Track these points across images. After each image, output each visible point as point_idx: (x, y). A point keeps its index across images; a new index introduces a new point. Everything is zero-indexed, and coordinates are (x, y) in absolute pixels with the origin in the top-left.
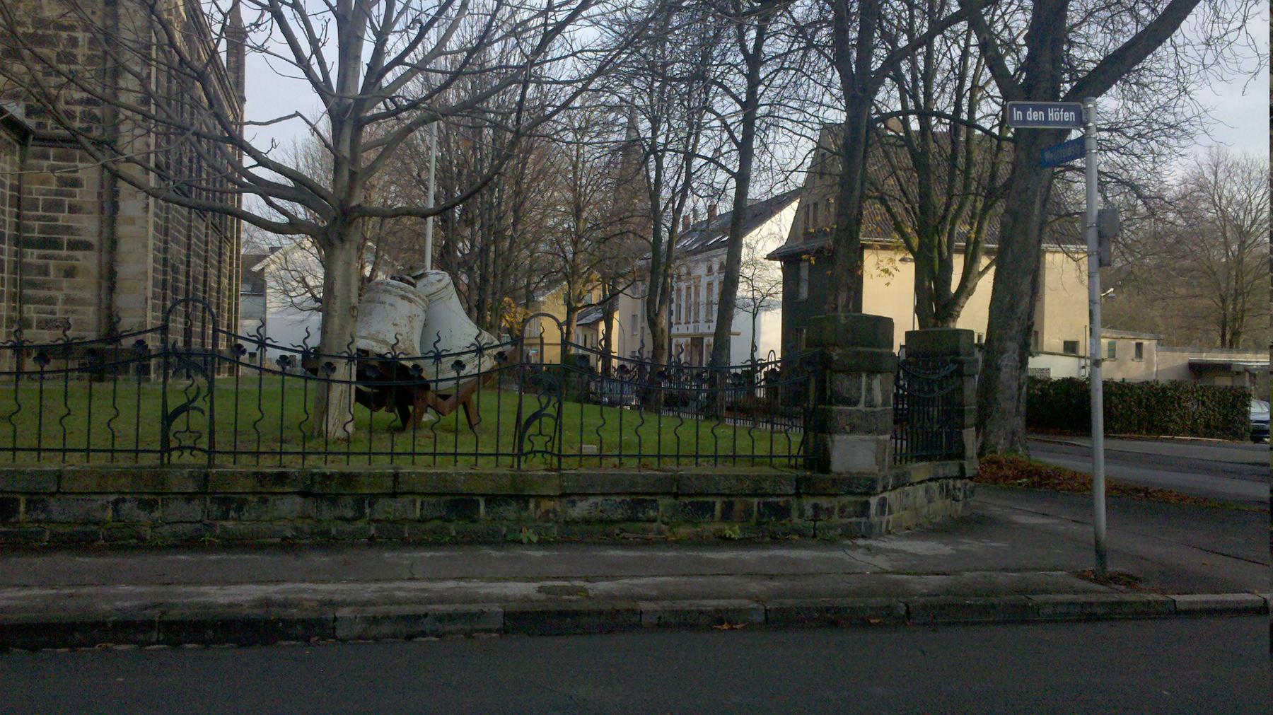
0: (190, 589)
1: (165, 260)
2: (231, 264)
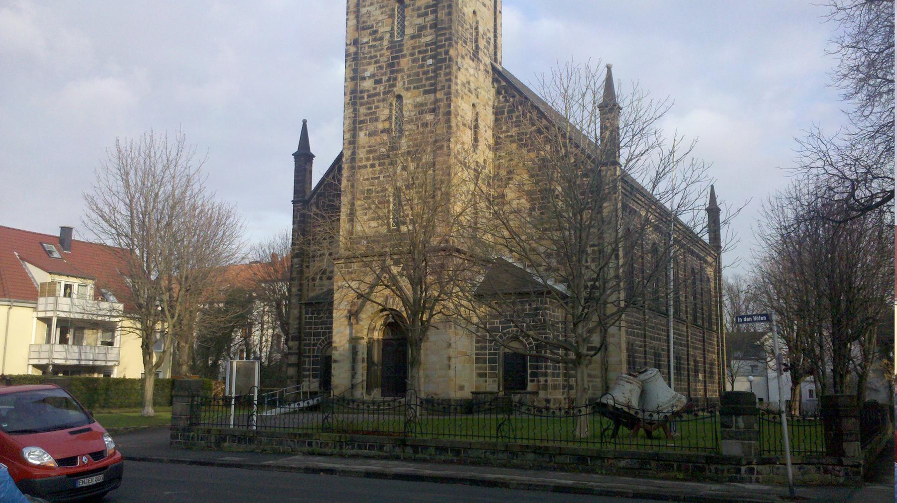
2: (718, 345)
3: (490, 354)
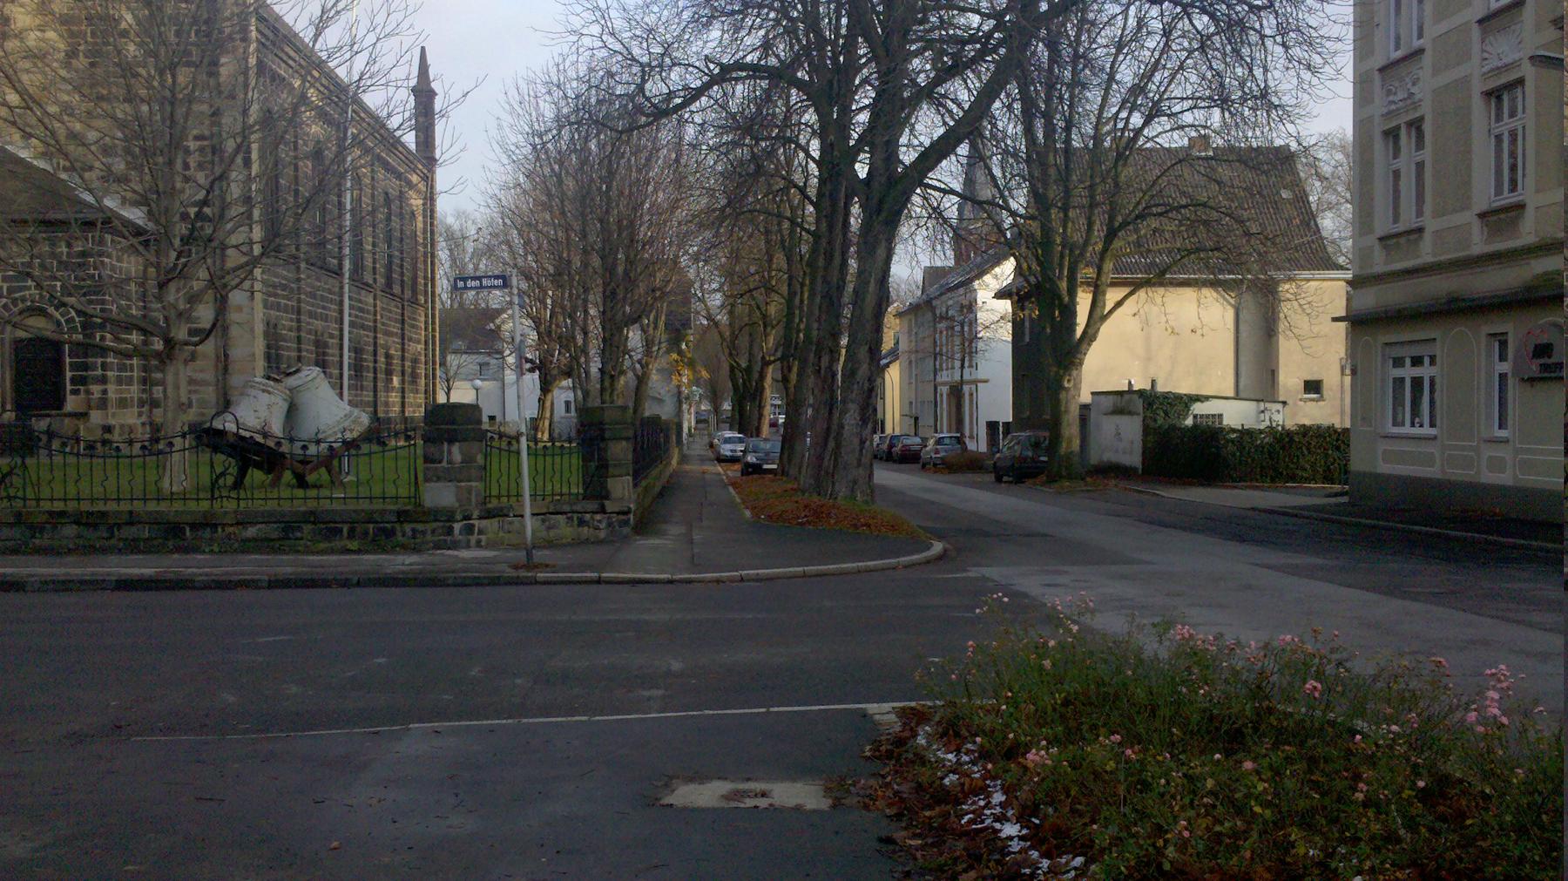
2: (426, 329)
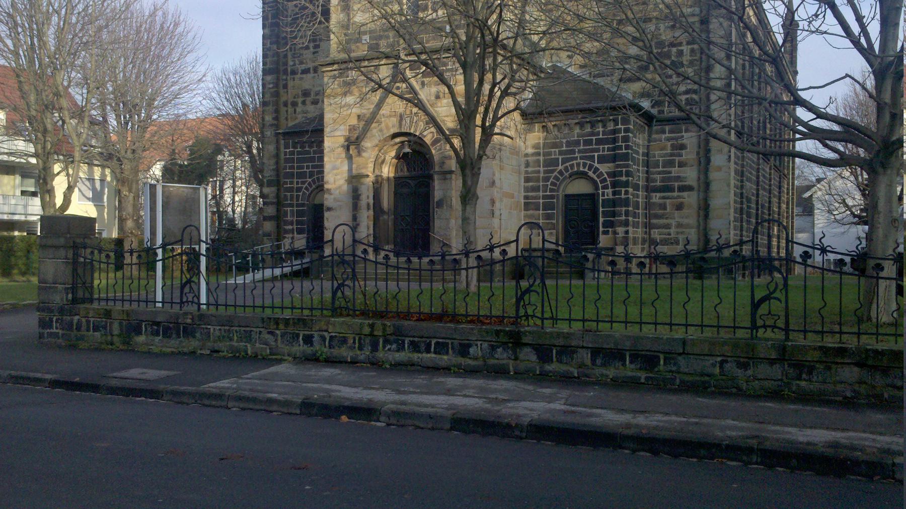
0: (778, 428)
1: (742, 194)
3: (544, 197)
